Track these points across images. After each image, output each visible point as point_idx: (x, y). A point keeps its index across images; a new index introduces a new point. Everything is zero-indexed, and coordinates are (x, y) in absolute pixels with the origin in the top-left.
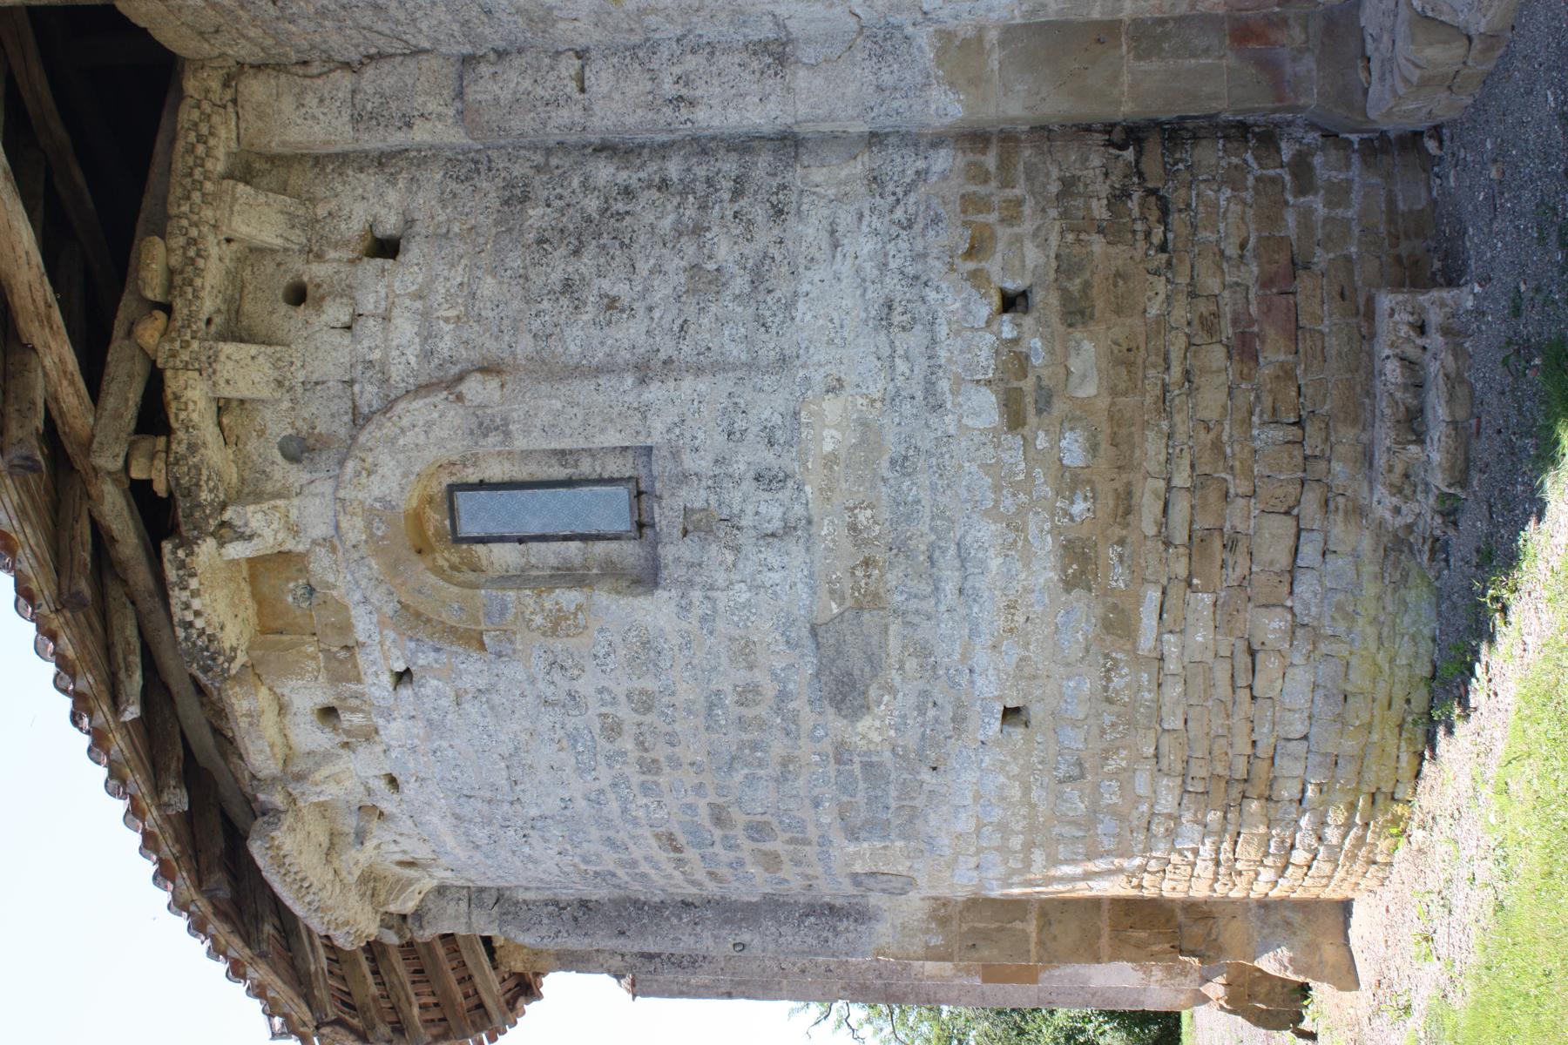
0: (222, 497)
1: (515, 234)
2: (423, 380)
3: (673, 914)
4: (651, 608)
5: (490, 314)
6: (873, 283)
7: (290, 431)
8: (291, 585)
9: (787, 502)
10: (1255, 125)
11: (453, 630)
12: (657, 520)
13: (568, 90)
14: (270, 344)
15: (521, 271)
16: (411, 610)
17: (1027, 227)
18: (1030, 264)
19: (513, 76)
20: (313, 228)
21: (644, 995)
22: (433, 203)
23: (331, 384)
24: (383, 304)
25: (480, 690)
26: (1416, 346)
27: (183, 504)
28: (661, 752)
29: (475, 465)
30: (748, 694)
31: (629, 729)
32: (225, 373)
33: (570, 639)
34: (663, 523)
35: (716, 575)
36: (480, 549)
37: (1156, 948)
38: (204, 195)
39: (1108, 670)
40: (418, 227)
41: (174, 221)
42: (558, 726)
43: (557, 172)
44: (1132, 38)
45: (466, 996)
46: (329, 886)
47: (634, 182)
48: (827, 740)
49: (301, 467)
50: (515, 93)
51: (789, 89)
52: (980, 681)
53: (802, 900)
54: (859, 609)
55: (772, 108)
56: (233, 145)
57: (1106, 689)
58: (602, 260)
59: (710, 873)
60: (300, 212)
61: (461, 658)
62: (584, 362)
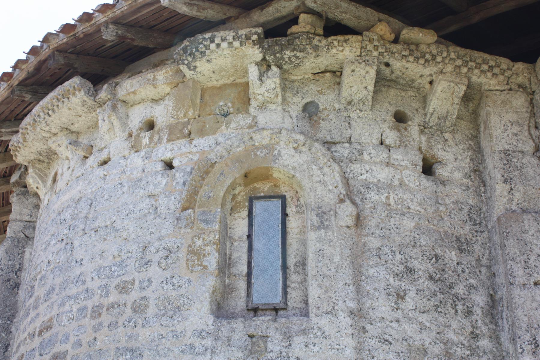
1: (440, 242)
2: (352, 182)
5: (392, 223)
7: (321, 107)
8: (230, 104)
11: (196, 192)
12: (260, 318)
15: (418, 244)
16: (210, 169)
20: (438, 130)
22: (456, 197)
23: (349, 131)
25: (157, 208)
27: (284, 40)
28: (106, 319)
29: (297, 212)
32: (358, 69)
33: (185, 261)
34: (258, 322)
36: (245, 213)
38: (459, 67)
40: (441, 187)
41: (446, 49)
42: (130, 255)
43: (477, 270)
46: (47, 129)
47: (475, 317)
49: (300, 112)
50: (531, 243)
56: (486, 87)
58: (427, 293)
59: (23, 354)
60: (447, 123)
61: (178, 197)
62: (363, 277)
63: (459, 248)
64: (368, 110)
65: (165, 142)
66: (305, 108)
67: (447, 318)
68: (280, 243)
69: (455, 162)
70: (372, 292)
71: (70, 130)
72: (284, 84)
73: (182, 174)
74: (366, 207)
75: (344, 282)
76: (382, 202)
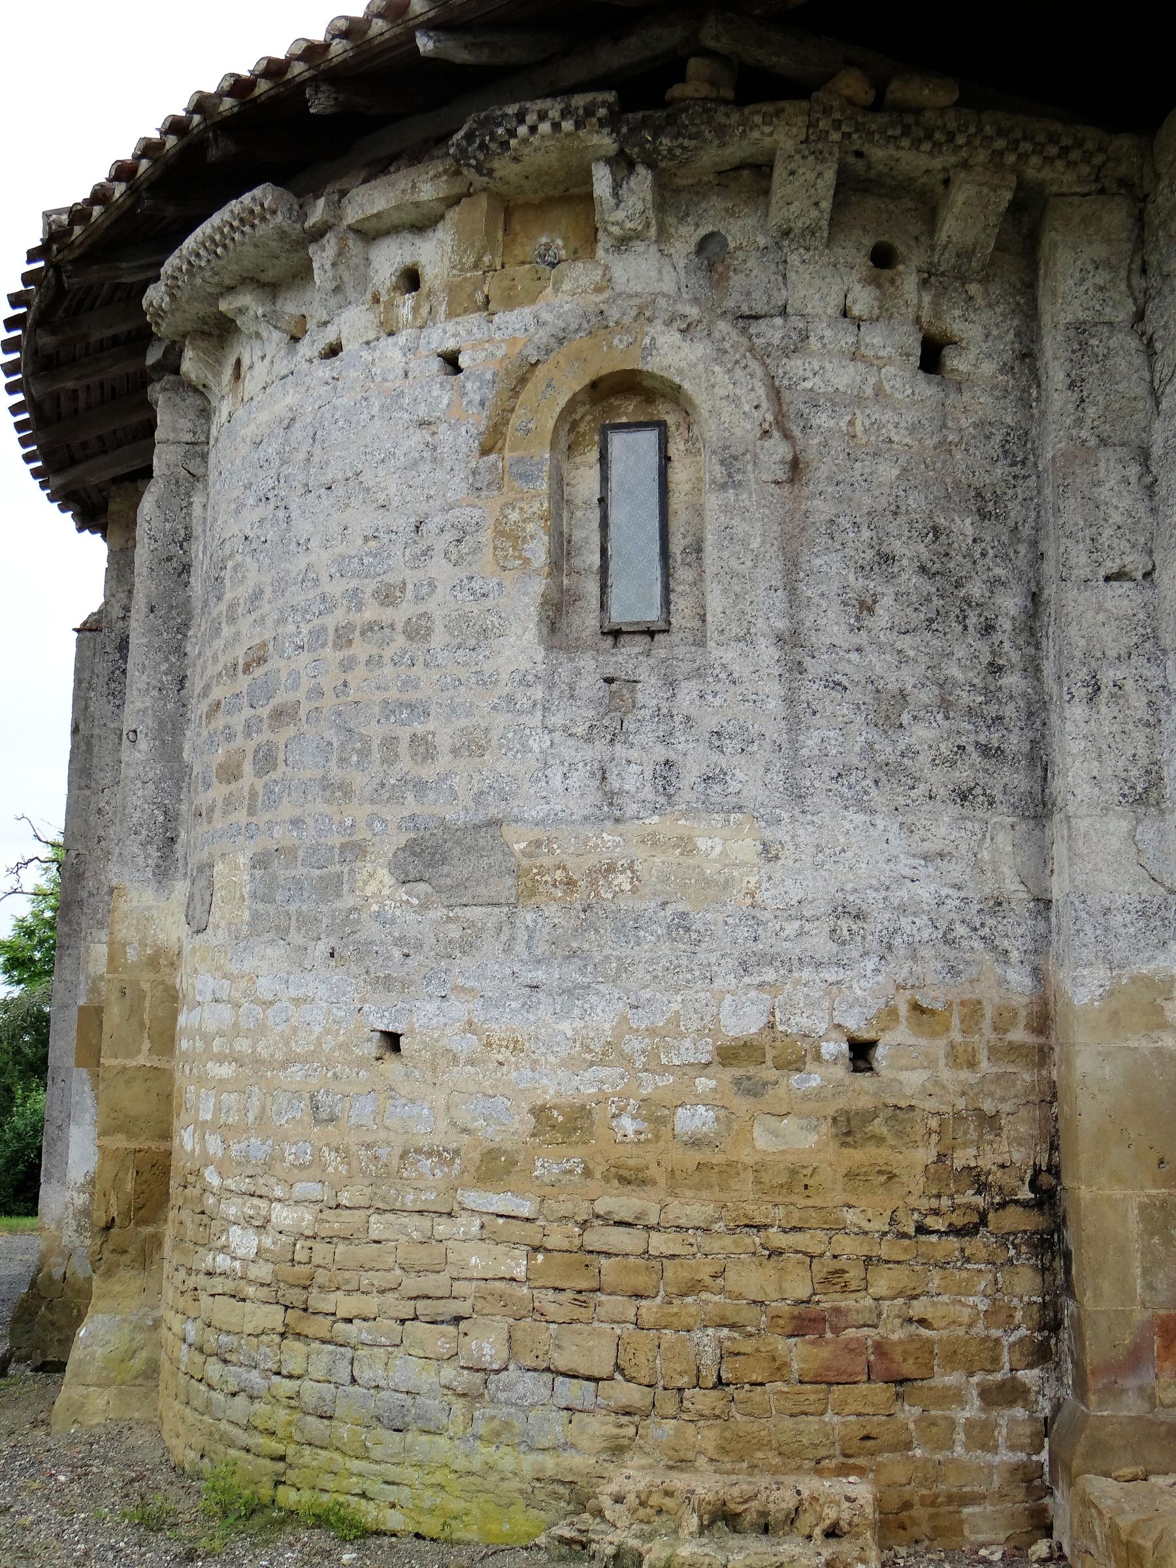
0: (663, 165)
2: (786, 395)
3: (172, 665)
4: (525, 643)
5: (857, 473)
6: (885, 899)
7: (732, 245)
8: (559, 242)
9: (641, 796)
10: (1058, 1340)
12: (623, 650)
13: (1109, 564)
14: (830, 225)
17: (946, 1075)
18: (905, 1076)
19: (1125, 503)
20: (956, 278)
21: (79, 641)
23: (784, 292)
24: (869, 353)
26: (812, 1527)
28: (361, 650)
30: (424, 748)
31: (387, 615)
35: (560, 715)
36: (594, 455)
37: (113, 1200)
38: (1001, 153)
39: (440, 1155)
42: (393, 537)
44: (1165, 1201)
45: (84, 445)
47: (997, 637)
48: (369, 836)
50: (1106, 504)
51: (1106, 810)
52: (431, 1007)
53: (184, 808)
54: (517, 873)
55: (1085, 790)
56: (1055, 189)
57: (418, 1151)
59: (219, 704)
60: (974, 264)
62: (802, 575)
63: (979, 510)
64: (821, 248)
65: (443, 319)
66: (703, 245)
67: (947, 640)
68: (657, 512)
69: (985, 341)
70: (816, 599)
71: (258, 281)
72: (662, 196)
73: (478, 384)
74: (811, 442)
75: (768, 585)
76: (840, 431)
